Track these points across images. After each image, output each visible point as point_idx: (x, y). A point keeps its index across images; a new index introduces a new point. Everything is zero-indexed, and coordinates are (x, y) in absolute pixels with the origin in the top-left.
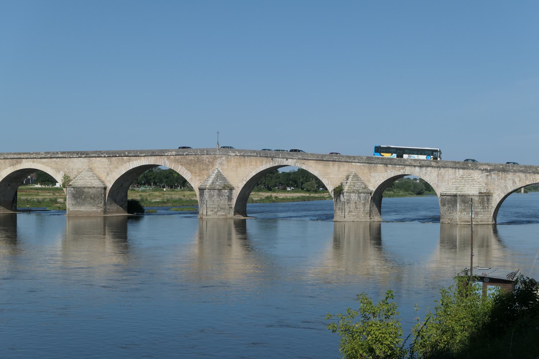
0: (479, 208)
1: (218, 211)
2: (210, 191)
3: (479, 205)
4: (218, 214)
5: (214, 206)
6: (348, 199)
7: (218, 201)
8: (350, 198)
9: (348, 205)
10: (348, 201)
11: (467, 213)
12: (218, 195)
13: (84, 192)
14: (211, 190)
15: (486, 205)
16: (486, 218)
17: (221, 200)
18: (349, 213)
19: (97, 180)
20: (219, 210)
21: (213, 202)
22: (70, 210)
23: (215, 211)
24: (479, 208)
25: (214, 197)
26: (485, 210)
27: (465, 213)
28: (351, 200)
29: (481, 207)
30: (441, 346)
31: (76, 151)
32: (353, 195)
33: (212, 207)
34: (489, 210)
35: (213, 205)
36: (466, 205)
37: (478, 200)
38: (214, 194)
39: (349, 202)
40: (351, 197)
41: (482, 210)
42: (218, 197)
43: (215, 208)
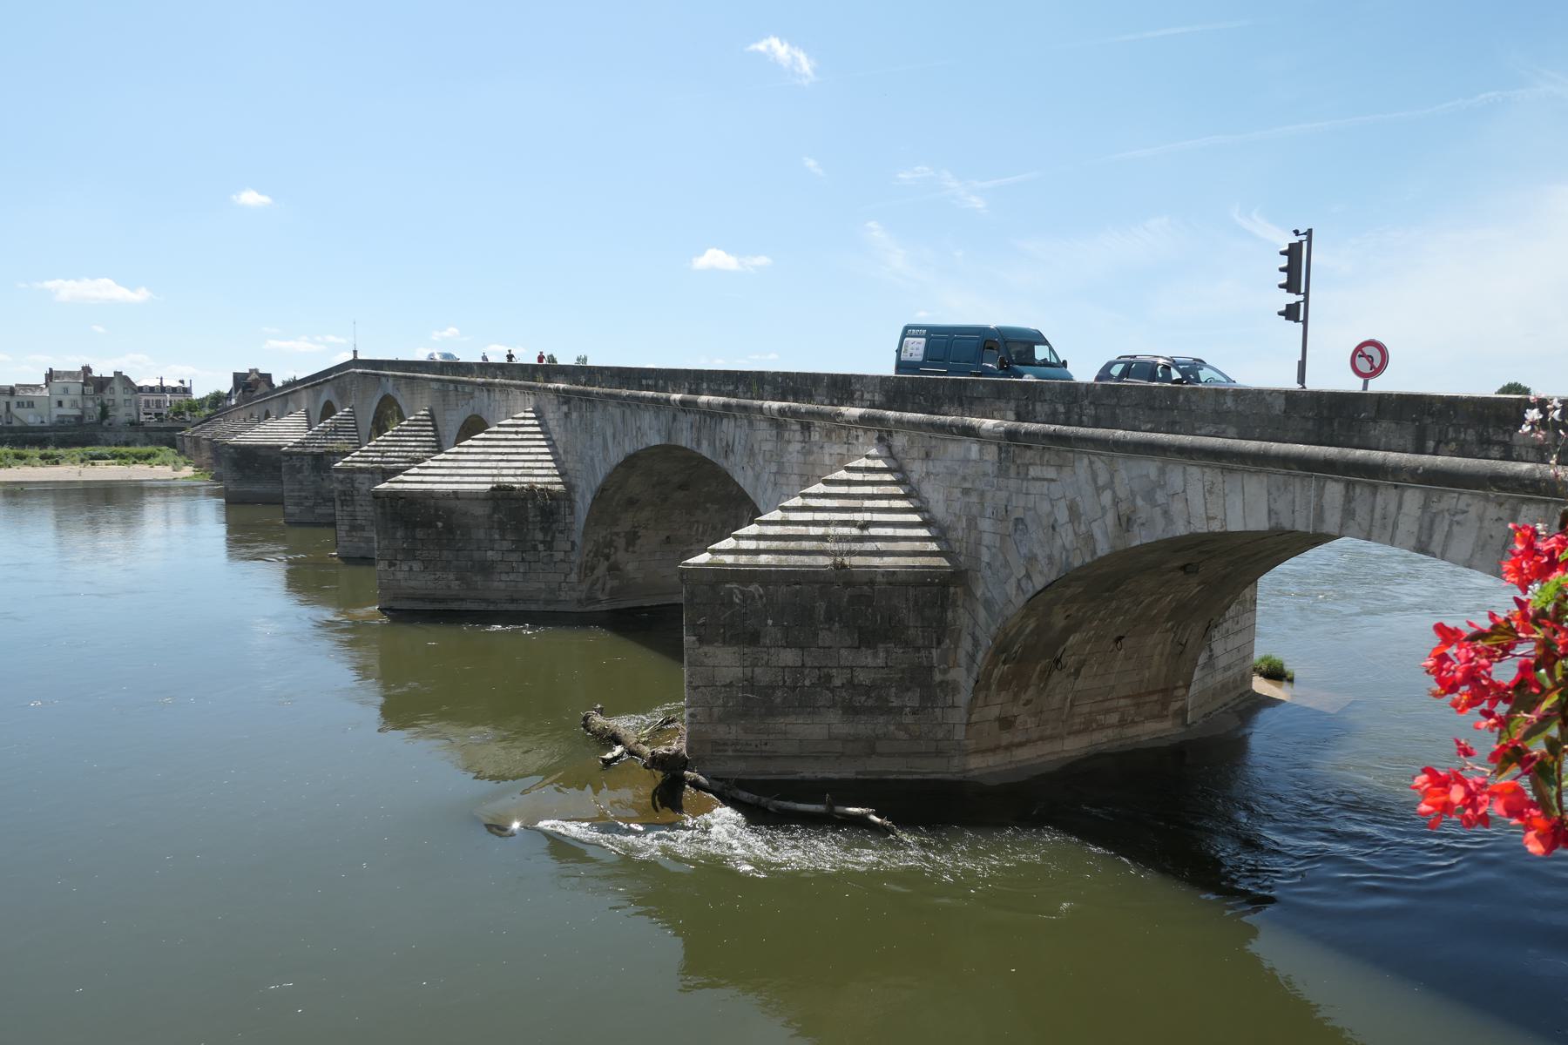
0: (496, 546)
1: (316, 505)
2: (291, 459)
3: (497, 537)
4: (316, 511)
5: (303, 494)
6: (344, 491)
7: (314, 482)
8: (353, 487)
9: (345, 508)
10: (343, 498)
11: (426, 568)
12: (312, 468)
13: (259, 456)
14: (294, 457)
15: (540, 536)
16: (543, 586)
17: (323, 479)
18: (350, 531)
19: (531, 422)
20: (320, 503)
21: (301, 483)
22: (230, 489)
23: (308, 504)
24: (496, 546)
25: (303, 472)
26: (528, 557)
27: (417, 566)
28: (355, 493)
29: (506, 545)
30: (1527, 563)
31: (776, 374)
32: (365, 478)
33: (299, 496)
34: (559, 556)
35: (300, 490)
36: (420, 534)
37: (490, 516)
38: (303, 465)
39: (348, 498)
40: (357, 485)
41: (514, 557)
42: (315, 474)
43: (306, 498)
